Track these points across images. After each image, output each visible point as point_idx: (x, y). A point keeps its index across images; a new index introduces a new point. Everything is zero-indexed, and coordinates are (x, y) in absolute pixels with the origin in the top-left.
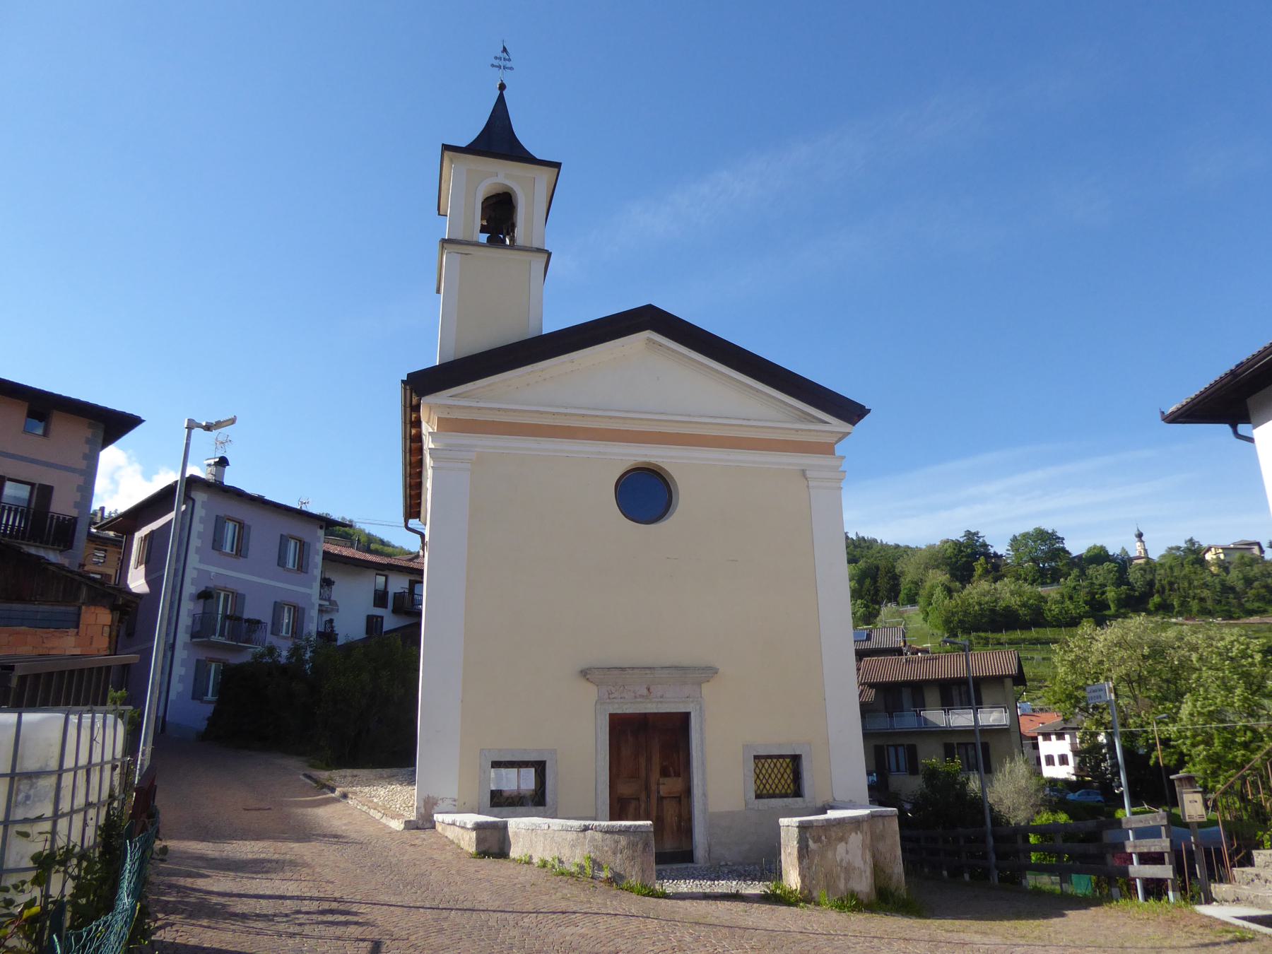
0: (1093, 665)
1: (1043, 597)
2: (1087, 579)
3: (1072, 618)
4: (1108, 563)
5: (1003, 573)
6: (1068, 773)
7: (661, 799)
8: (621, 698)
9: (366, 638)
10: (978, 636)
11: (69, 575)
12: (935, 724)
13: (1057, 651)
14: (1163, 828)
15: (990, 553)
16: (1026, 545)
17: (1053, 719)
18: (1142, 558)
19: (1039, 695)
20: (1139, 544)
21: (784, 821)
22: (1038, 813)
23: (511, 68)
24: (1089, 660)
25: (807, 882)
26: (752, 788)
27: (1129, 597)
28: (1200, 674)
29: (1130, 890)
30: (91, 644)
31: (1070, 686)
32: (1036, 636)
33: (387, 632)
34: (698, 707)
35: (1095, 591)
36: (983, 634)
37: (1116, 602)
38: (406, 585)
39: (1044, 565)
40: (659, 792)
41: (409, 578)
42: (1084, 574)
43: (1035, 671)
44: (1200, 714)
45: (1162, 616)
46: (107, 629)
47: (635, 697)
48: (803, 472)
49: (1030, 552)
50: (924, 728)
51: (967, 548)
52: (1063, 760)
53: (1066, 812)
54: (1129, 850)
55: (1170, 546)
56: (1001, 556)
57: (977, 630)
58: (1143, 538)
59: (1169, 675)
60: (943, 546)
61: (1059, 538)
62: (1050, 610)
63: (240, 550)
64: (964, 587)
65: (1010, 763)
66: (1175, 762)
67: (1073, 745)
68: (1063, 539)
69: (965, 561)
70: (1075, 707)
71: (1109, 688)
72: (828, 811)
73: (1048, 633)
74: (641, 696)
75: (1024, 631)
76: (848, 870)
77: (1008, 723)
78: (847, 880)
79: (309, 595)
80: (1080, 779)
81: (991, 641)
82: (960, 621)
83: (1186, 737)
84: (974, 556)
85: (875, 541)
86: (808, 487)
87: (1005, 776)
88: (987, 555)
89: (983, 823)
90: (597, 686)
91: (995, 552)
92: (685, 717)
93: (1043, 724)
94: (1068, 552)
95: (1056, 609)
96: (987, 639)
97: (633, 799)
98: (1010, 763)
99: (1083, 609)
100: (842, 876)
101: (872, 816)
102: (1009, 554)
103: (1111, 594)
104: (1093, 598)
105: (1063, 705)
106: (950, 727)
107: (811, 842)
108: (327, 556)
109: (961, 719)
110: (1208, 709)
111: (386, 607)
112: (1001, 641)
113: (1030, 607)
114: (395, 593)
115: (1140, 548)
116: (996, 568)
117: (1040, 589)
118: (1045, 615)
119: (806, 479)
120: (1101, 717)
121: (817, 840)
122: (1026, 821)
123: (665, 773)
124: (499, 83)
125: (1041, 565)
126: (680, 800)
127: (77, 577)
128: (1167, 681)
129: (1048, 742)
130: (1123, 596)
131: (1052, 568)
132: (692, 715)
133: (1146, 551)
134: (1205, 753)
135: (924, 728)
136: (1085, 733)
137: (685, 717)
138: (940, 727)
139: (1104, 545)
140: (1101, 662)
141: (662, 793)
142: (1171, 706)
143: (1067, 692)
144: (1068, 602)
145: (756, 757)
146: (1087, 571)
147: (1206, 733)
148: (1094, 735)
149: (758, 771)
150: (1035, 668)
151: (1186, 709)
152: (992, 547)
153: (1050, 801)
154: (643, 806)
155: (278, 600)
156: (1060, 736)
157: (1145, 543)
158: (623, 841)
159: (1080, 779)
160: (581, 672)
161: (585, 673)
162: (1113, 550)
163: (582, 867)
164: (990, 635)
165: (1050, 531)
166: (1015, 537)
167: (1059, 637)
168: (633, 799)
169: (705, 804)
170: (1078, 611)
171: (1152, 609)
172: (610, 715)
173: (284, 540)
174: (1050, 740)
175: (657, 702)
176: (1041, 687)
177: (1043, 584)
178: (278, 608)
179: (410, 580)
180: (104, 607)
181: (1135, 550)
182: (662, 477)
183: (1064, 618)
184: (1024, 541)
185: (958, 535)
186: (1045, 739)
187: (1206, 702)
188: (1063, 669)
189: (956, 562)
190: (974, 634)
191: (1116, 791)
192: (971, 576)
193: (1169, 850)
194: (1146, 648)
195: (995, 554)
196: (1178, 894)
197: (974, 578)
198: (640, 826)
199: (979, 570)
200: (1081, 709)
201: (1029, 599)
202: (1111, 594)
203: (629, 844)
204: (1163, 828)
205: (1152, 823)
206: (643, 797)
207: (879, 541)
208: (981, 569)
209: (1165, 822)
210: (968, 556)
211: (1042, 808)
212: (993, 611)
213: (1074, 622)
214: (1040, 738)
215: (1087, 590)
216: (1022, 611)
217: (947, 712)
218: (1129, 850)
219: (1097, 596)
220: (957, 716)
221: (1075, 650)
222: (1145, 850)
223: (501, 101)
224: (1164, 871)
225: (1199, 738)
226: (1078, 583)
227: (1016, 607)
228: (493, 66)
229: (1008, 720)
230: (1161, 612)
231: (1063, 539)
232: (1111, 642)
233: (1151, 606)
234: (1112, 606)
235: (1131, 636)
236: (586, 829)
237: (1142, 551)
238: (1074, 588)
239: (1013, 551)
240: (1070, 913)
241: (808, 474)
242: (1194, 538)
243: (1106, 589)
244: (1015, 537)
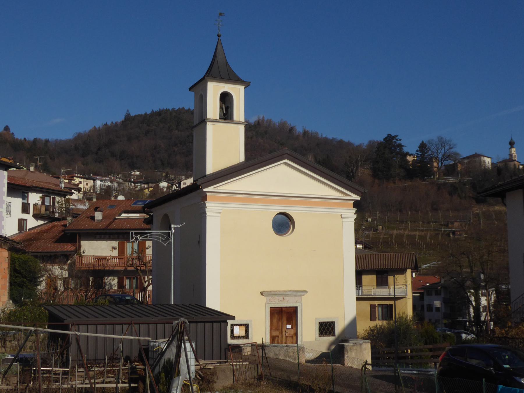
7: (286, 337)
8: (274, 302)
34: (300, 305)
46: (7, 259)
47: (279, 301)
50: (361, 296)
92: (296, 308)
97: (277, 337)
111: (29, 213)
132: (298, 307)
135: (361, 296)
168: (277, 337)
169: (302, 339)
185: (380, 138)
239: (420, 152)
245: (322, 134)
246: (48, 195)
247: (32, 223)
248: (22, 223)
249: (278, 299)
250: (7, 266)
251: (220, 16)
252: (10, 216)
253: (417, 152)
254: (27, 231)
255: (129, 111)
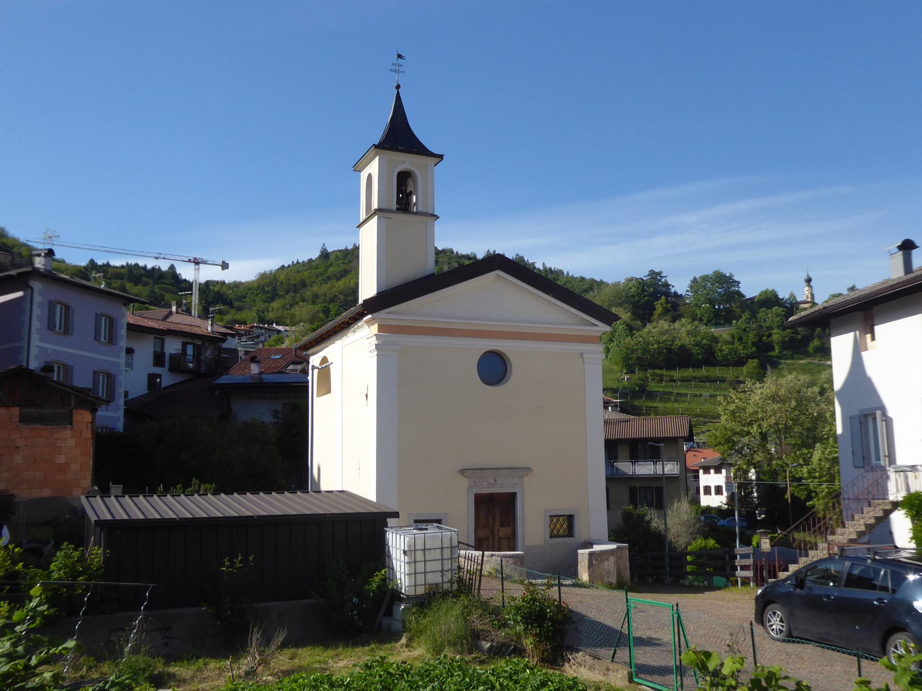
0: (749, 415)
1: (716, 338)
2: (756, 322)
3: (740, 358)
4: (777, 307)
5: (681, 312)
6: (721, 502)
7: (500, 538)
9: (148, 393)
10: (654, 373)
11: (64, 388)
12: (624, 472)
13: (722, 402)
14: (751, 554)
15: (671, 293)
16: (704, 287)
17: (712, 455)
18: (808, 302)
19: (703, 430)
20: (807, 288)
21: (580, 551)
22: (694, 539)
23: (403, 72)
24: (747, 410)
25: (592, 578)
26: (548, 532)
27: (792, 340)
28: (831, 427)
29: (735, 584)
30: (81, 435)
31: (729, 432)
32: (706, 374)
33: (164, 388)
35: (763, 333)
36: (658, 372)
37: (780, 344)
38: (180, 347)
39: (719, 307)
40: (499, 535)
41: (182, 340)
42: (755, 316)
43: (702, 407)
44: (827, 459)
45: (820, 358)
48: (581, 355)
49: (708, 294)
51: (649, 286)
52: (719, 490)
53: (714, 539)
54: (736, 564)
55: (832, 293)
56: (681, 295)
57: (653, 367)
58: (812, 284)
59: (810, 425)
60: (628, 285)
61: (735, 282)
62: (721, 350)
63: (67, 330)
64: (644, 326)
65: (678, 503)
66: (805, 497)
67: (728, 478)
68: (739, 283)
69: (648, 300)
70: (731, 449)
71: (735, 486)
72: (594, 546)
73: (717, 372)
74: (492, 484)
75: (695, 369)
76: (608, 573)
77: (678, 473)
78: (608, 578)
79: (41, 340)
80: (730, 508)
81: (665, 378)
82: (638, 358)
83: (815, 478)
84: (656, 295)
85: (561, 272)
86: (584, 363)
87: (673, 513)
88: (667, 294)
89: (665, 549)
90: (469, 479)
91: (675, 292)
92: (513, 496)
93: (704, 458)
94: (742, 296)
95: (726, 349)
96: (661, 376)
98: (678, 503)
99: (750, 351)
100: (606, 576)
101: (618, 548)
102: (688, 295)
103: (777, 335)
104: (760, 340)
105: (722, 447)
106: (635, 475)
107: (594, 561)
108: (132, 328)
109: (645, 469)
110: (832, 456)
112: (675, 378)
113: (702, 347)
114: (171, 354)
115: (807, 292)
116: (675, 307)
117: (713, 330)
118: (716, 355)
119: (583, 358)
120: (752, 458)
121: (597, 560)
122: (685, 544)
123: (502, 525)
124: (395, 85)
125: (717, 307)
126: (510, 539)
127: (69, 390)
128: (808, 429)
129: (707, 475)
130: (787, 339)
131: (725, 309)
132: (518, 493)
133: (812, 295)
134: (827, 490)
136: (738, 470)
137: (513, 496)
138: (628, 475)
139: (776, 290)
140: (756, 413)
141: (501, 536)
142: (806, 452)
143: (727, 437)
144: (737, 343)
145: (551, 516)
146: (757, 315)
147: (831, 474)
148: (746, 472)
149: (552, 527)
150: (702, 405)
151: (817, 455)
152: (673, 287)
153: (704, 531)
154: (490, 542)
155: (96, 370)
156: (718, 470)
157: (813, 288)
158: (511, 561)
159: (730, 508)
160: (460, 471)
161: (463, 472)
162: (783, 294)
163: (490, 573)
164: (664, 372)
165: (728, 275)
166: (695, 279)
167: (727, 376)
170: (746, 352)
171: (812, 351)
172: (475, 494)
173: (98, 317)
174: (709, 473)
175: (500, 487)
176: (706, 423)
177: (717, 324)
178: (96, 374)
179: (182, 342)
180: (87, 410)
181: (802, 294)
182: (503, 359)
183: (732, 358)
184: (703, 284)
185: (642, 273)
186: (705, 473)
187: (833, 449)
188: (725, 417)
189: (639, 301)
190: (650, 371)
191: (758, 518)
192: (652, 315)
193: (752, 564)
194: (793, 402)
195: (675, 293)
196: (755, 584)
197: (654, 317)
198: (519, 554)
199: (659, 310)
200: (736, 451)
201: (703, 339)
202: (777, 335)
203: (514, 562)
204: (751, 554)
205: (747, 552)
206: (491, 538)
207: (565, 273)
208: (661, 309)
209: (752, 552)
210: (650, 295)
211: (698, 535)
212: (669, 350)
213: (740, 362)
214: (701, 471)
215: (755, 332)
216: (695, 350)
217: (634, 463)
218: (736, 564)
219: (764, 338)
220: (641, 467)
221: (736, 401)
222: (743, 564)
223: (398, 98)
224: (749, 574)
225: (824, 479)
226: (748, 325)
227: (690, 346)
228: (391, 70)
229: (679, 471)
230: (819, 354)
231: (739, 283)
232: (766, 396)
233: (810, 349)
234: (776, 347)
235: (782, 392)
236: (492, 555)
237: (809, 295)
238: (745, 330)
239: (692, 293)
240: (706, 593)
241: (585, 356)
242: (856, 286)
243: (772, 331)
244: (695, 279)
245: (568, 272)
246: (191, 341)
247: (167, 379)
248: (152, 378)
249: (488, 482)
250: (90, 436)
251: (399, 59)
252: (132, 369)
253: (687, 293)
254: (162, 389)
255: (325, 245)
